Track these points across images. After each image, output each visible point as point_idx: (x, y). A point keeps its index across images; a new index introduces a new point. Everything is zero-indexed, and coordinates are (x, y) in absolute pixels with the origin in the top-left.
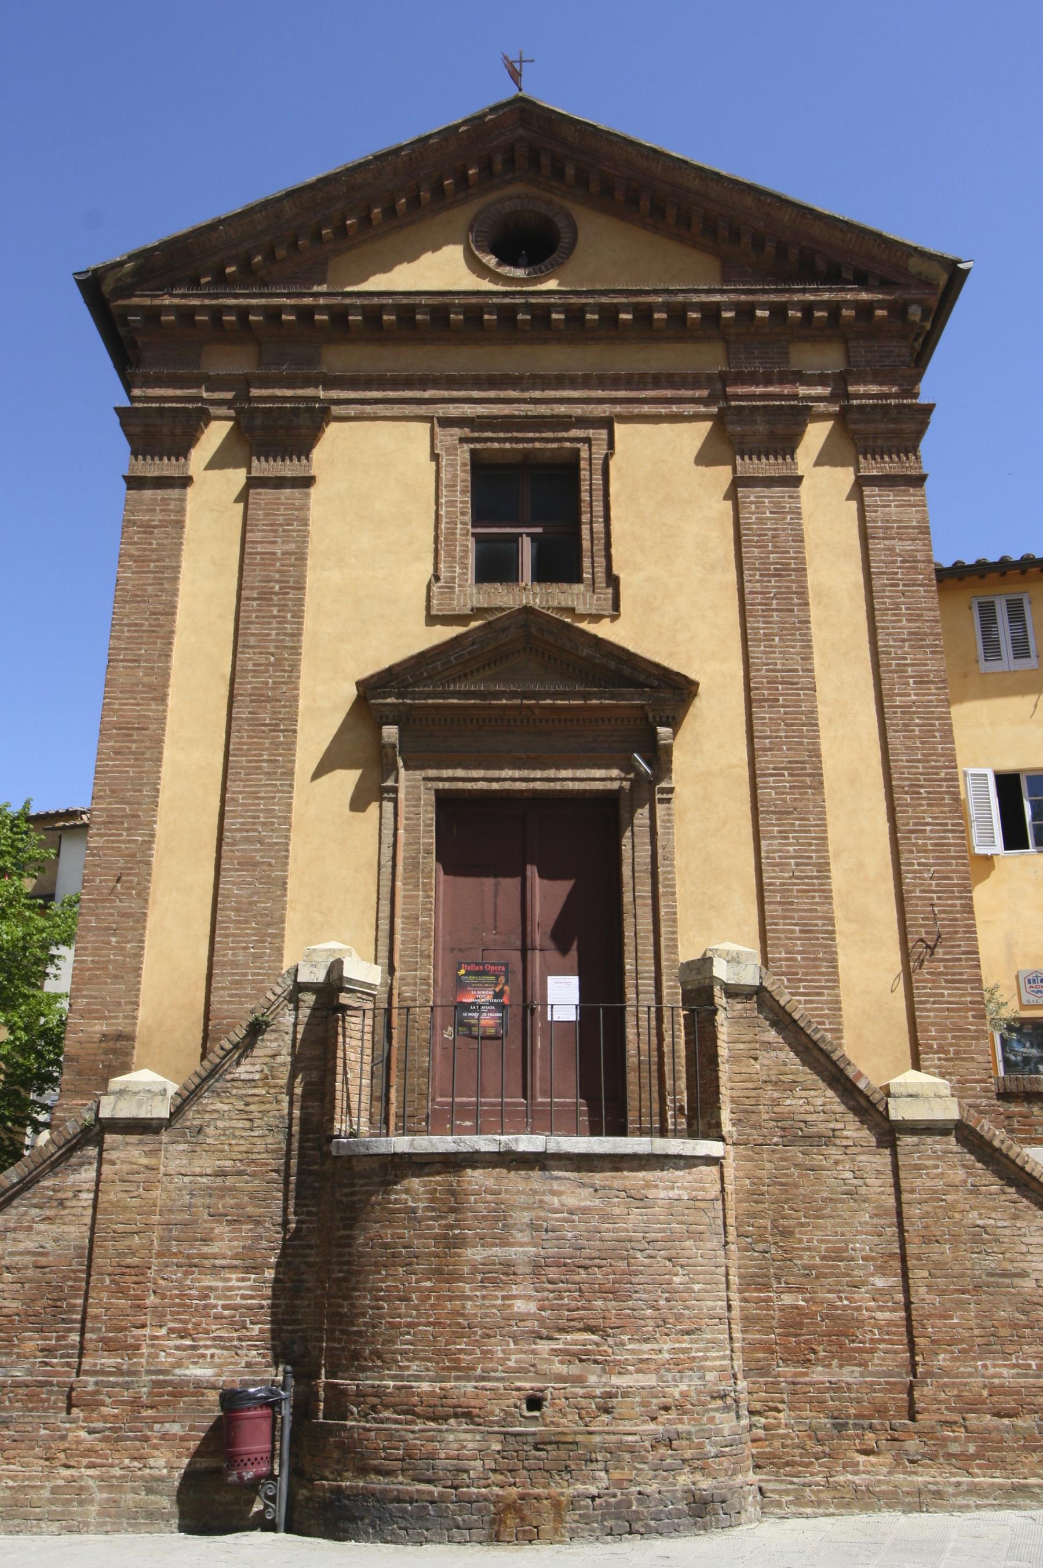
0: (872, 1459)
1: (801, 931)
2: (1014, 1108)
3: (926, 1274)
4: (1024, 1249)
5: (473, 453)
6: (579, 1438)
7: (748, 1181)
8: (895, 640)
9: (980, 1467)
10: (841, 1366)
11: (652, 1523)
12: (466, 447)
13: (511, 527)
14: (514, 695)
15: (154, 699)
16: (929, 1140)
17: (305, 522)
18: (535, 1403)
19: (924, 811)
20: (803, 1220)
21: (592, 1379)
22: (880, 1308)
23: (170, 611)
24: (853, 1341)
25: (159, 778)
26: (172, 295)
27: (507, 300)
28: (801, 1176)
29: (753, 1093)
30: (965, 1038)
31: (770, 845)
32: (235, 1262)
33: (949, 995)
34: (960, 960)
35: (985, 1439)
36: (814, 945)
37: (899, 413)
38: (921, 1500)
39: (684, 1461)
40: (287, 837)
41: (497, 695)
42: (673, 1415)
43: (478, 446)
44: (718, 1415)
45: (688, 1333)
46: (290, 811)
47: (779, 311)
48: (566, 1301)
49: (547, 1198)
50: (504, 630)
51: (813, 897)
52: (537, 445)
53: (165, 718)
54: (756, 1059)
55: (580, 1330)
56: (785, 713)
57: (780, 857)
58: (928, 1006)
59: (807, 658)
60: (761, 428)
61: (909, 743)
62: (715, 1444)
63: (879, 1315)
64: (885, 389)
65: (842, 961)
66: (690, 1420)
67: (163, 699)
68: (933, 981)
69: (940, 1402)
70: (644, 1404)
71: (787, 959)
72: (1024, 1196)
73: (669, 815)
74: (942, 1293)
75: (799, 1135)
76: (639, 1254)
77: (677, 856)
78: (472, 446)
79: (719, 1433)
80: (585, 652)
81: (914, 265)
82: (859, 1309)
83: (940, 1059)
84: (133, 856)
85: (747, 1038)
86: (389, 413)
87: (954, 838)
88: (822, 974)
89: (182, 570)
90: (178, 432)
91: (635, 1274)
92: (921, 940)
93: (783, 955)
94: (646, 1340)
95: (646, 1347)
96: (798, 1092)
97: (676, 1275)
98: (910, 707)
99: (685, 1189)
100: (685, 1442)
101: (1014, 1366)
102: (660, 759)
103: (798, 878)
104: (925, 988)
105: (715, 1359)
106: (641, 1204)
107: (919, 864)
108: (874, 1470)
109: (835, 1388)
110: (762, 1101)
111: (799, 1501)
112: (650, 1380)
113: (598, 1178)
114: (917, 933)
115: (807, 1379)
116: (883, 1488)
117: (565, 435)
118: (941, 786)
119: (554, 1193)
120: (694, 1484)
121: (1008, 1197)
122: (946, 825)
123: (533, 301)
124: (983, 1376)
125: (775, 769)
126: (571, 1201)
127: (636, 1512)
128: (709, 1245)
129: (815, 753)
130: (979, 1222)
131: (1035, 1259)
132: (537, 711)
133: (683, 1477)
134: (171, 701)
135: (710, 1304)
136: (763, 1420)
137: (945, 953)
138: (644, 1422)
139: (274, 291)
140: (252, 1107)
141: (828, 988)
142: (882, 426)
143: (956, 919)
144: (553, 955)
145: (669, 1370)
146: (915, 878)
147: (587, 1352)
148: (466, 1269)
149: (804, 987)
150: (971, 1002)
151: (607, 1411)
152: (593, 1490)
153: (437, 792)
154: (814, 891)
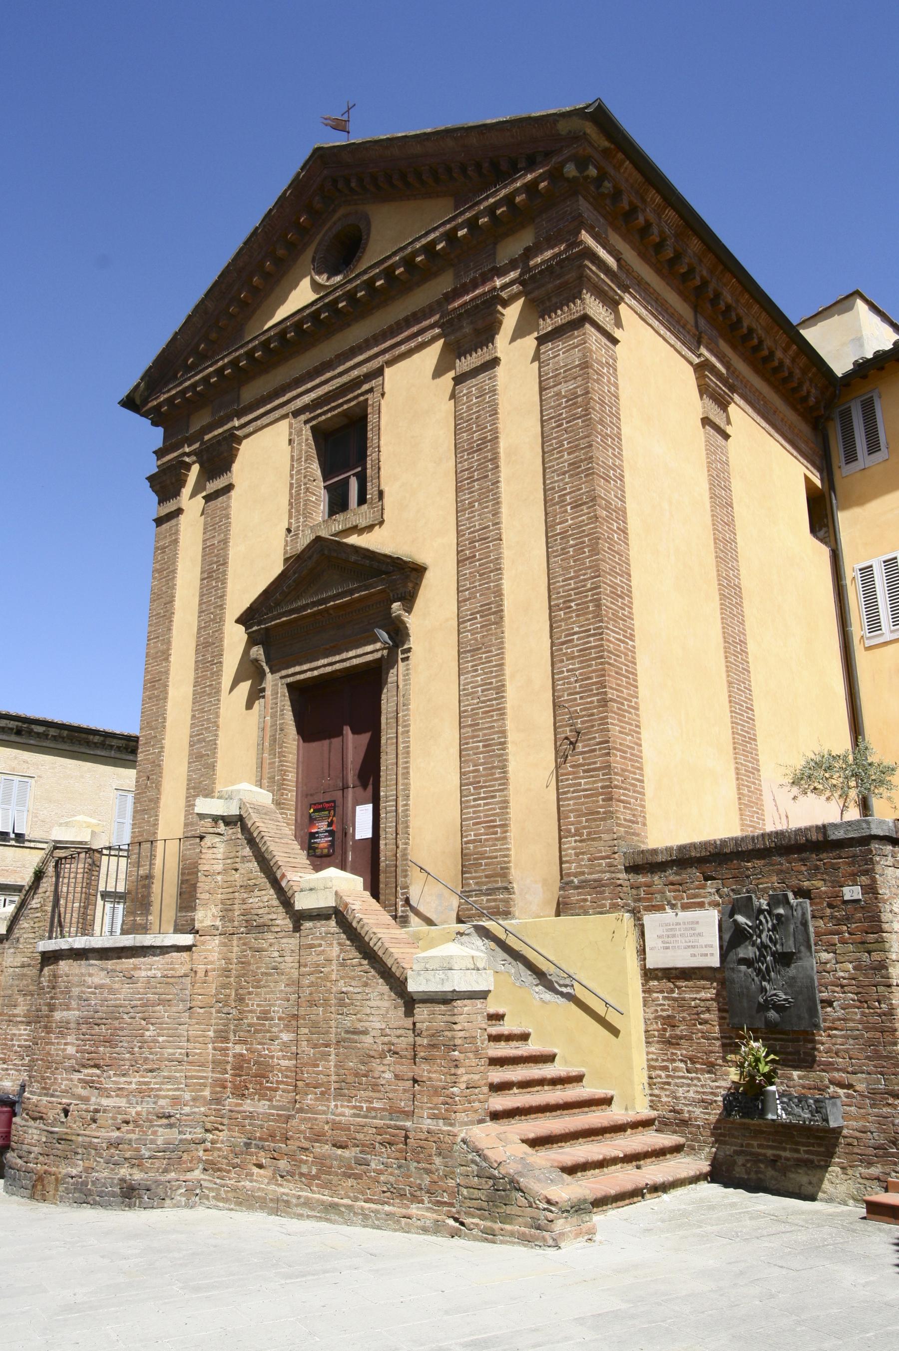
0: (262, 1171)
1: (484, 746)
2: (642, 879)
3: (306, 1031)
4: (368, 1011)
5: (312, 428)
6: (74, 1138)
7: (223, 961)
8: (558, 475)
9: (317, 1185)
10: (259, 1100)
11: (97, 1198)
12: (308, 426)
13: (338, 476)
14: (314, 604)
15: (164, 660)
16: (318, 924)
17: (228, 517)
18: (66, 1112)
19: (574, 623)
20: (251, 989)
21: (93, 1099)
22: (284, 1057)
23: (171, 601)
24: (267, 1082)
25: (166, 710)
26: (164, 393)
27: (314, 308)
28: (253, 956)
29: (231, 896)
30: (595, 820)
31: (466, 679)
32: (24, 1019)
33: (586, 783)
34: (594, 750)
35: (320, 1161)
36: (491, 756)
37: (562, 268)
38: (278, 1206)
39: (125, 1159)
40: (216, 735)
41: (305, 607)
42: (131, 1127)
43: (314, 423)
44: (161, 1130)
45: (151, 1071)
46: (218, 717)
47: (472, 224)
48: (87, 1047)
49: (86, 978)
50: (310, 558)
51: (492, 716)
52: (345, 407)
53: (169, 670)
54: (236, 870)
55: (92, 1066)
56: (480, 565)
57: (472, 688)
58: (569, 795)
59: (496, 513)
60: (467, 329)
61: (565, 565)
62: (149, 1149)
63: (282, 1062)
64: (556, 250)
65: (512, 767)
66: (139, 1131)
67: (167, 659)
68: (574, 773)
69: (301, 1132)
70: (114, 1118)
71: (473, 771)
72: (373, 967)
73: (408, 670)
74: (315, 1046)
75: (257, 927)
76: (125, 1016)
77: (412, 702)
78: (311, 424)
79: (153, 1142)
80: (353, 558)
81: (563, 127)
82: (272, 1057)
83: (576, 841)
84: (154, 762)
85: (232, 855)
86: (268, 421)
87: (595, 641)
88: (496, 779)
89: (178, 572)
90: (174, 480)
91: (122, 1029)
92: (567, 738)
93: (471, 768)
94: (124, 1075)
95: (123, 1079)
96: (257, 893)
97: (148, 1030)
98: (568, 531)
99: (158, 969)
100: (126, 1146)
101: (355, 1107)
102: (399, 634)
103: (483, 702)
104: (567, 780)
105: (169, 1090)
106: (129, 981)
107: (568, 671)
108: (259, 1181)
109: (251, 1116)
110: (236, 902)
111: (217, 1198)
112: (122, 1102)
113: (110, 964)
114: (563, 732)
115: (241, 1108)
116: (260, 1194)
117: (359, 391)
118: (586, 596)
119: (90, 975)
120: (131, 1175)
121: (363, 968)
122: (589, 630)
123: (327, 301)
124: (333, 1114)
125: (471, 615)
126: (97, 980)
127: (89, 1190)
128: (174, 1009)
129: (499, 593)
130: (344, 989)
131: (374, 1019)
132: (331, 612)
133: (124, 1170)
134: (172, 659)
135: (170, 1051)
136: (211, 1136)
137: (584, 747)
138: (113, 1130)
139: (204, 366)
140: (36, 925)
141: (500, 790)
142: (550, 286)
143: (592, 715)
144: (359, 790)
145: (135, 1096)
146: (564, 684)
147: (93, 1082)
148: (54, 1025)
149: (484, 792)
150: (602, 787)
151: (94, 1121)
152: (74, 1172)
153: (289, 686)
154: (493, 711)
